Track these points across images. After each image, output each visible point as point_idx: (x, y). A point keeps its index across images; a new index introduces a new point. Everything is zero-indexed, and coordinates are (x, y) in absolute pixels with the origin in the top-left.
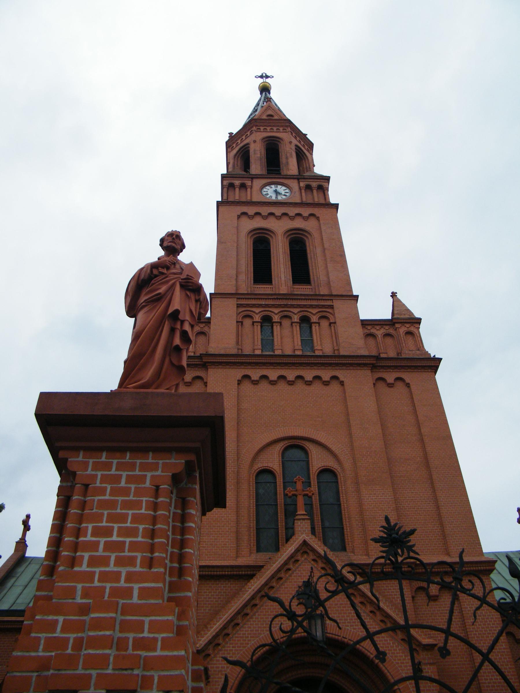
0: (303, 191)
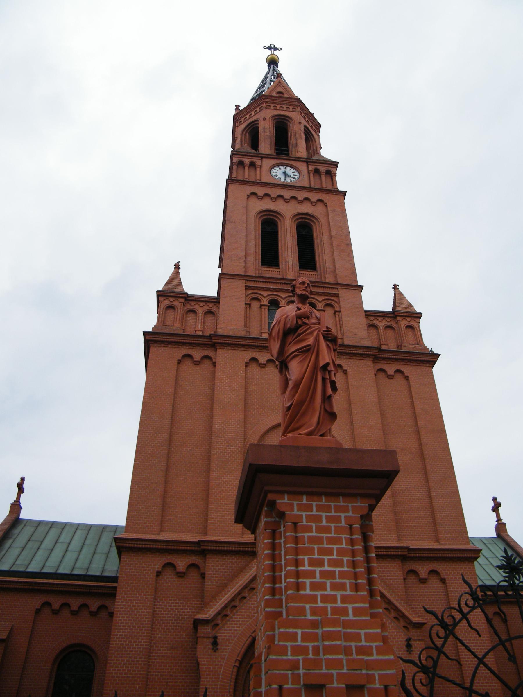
0: (312, 175)
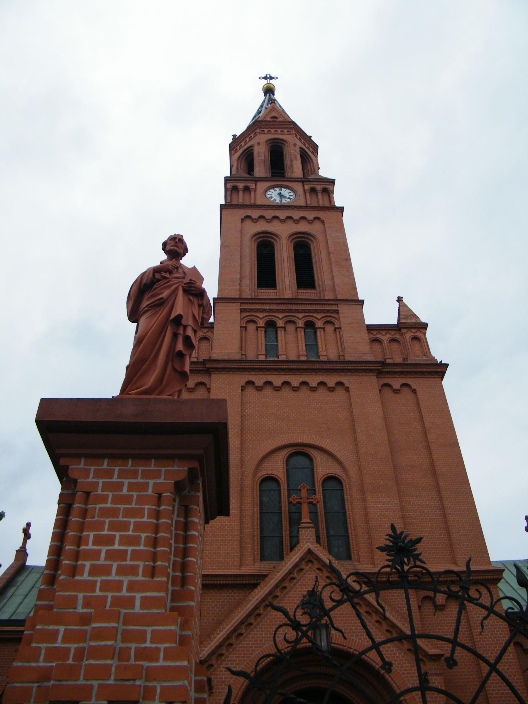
0: (308, 194)
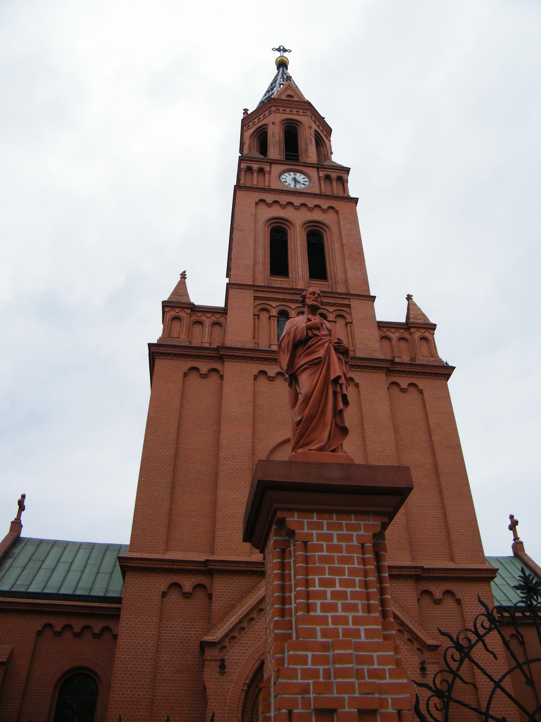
0: (322, 181)
